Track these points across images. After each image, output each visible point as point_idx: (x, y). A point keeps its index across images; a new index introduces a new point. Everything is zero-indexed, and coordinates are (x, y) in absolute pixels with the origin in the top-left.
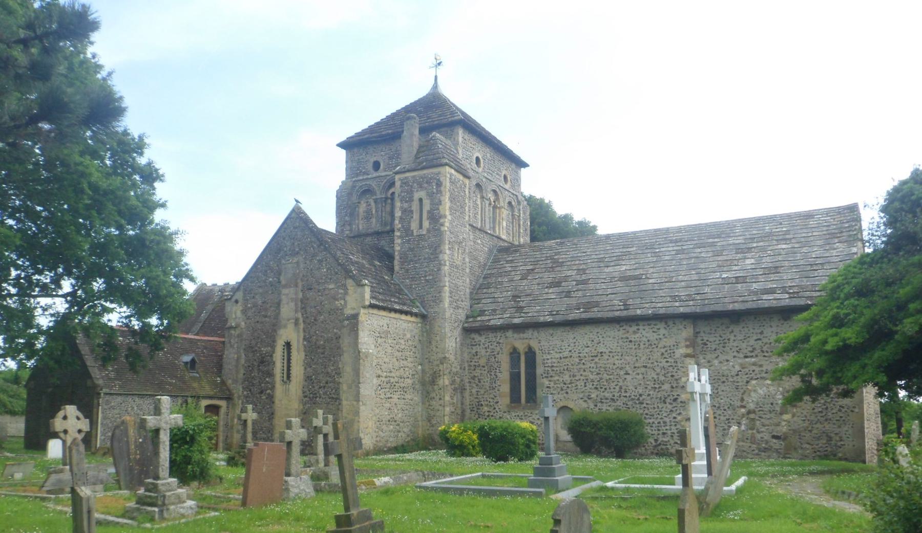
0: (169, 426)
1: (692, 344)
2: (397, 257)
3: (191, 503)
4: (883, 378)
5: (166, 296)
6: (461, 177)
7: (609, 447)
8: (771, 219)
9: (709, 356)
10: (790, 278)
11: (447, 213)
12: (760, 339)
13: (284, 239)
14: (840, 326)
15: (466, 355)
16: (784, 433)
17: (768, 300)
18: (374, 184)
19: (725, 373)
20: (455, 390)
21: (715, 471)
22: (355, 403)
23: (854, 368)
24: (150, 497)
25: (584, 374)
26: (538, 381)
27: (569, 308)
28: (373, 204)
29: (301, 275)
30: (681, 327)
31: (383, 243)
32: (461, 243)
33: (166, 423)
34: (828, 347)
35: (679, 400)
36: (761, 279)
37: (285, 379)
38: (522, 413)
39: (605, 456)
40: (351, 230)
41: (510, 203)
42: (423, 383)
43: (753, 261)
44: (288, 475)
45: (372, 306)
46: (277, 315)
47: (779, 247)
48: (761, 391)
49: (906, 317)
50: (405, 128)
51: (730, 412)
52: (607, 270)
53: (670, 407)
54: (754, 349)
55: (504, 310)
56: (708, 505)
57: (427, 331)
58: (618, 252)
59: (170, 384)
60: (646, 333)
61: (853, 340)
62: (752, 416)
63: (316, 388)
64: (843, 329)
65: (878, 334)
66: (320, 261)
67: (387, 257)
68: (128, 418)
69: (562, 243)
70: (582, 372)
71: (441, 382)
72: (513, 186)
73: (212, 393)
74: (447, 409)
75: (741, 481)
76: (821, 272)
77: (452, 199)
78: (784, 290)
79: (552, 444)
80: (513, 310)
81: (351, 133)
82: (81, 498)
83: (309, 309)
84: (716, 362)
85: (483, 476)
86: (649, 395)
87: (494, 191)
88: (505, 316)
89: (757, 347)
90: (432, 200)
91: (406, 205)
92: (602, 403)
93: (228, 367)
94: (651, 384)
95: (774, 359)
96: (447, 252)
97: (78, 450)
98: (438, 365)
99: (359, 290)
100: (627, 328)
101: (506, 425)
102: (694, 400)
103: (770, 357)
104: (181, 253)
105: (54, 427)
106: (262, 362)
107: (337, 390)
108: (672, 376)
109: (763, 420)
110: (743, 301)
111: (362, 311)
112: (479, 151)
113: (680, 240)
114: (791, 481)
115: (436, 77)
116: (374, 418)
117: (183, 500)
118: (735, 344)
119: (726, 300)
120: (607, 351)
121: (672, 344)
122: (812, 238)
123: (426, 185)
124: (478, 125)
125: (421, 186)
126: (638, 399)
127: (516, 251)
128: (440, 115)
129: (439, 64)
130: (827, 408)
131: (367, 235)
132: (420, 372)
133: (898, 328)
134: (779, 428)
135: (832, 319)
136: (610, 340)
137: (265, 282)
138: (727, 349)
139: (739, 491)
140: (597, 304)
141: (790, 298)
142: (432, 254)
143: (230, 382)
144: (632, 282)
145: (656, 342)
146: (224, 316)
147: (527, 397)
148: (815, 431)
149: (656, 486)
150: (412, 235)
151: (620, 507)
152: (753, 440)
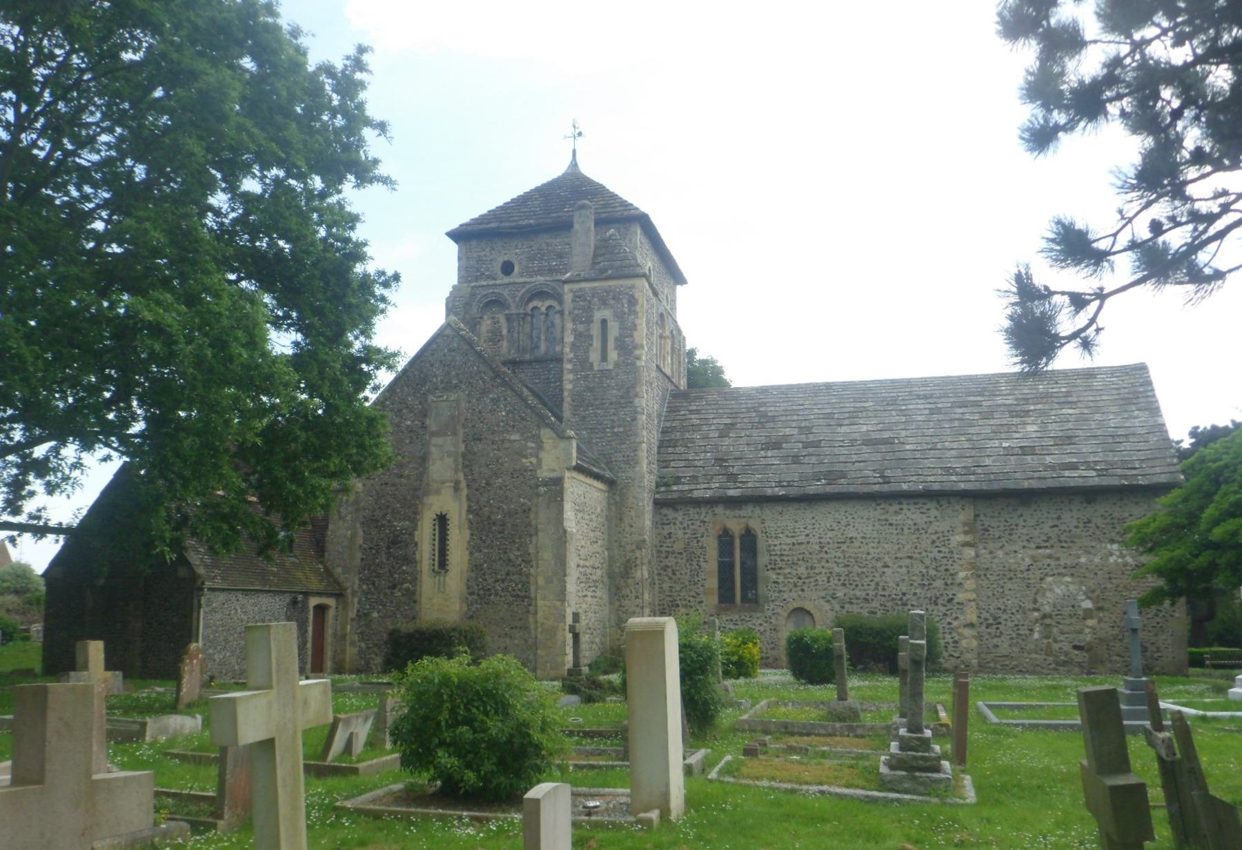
1: (970, 529)
9: (991, 545)
16: (1089, 643)
17: (1073, 478)
18: (506, 293)
19: (1013, 567)
22: (558, 603)
27: (803, 478)
29: (462, 419)
30: (958, 507)
35: (955, 601)
36: (1054, 450)
38: (735, 617)
42: (611, 575)
45: (578, 469)
46: (422, 474)
47: (1064, 411)
48: (1058, 591)
53: (943, 609)
57: (616, 503)
58: (849, 406)
60: (911, 515)
62: (1048, 621)
63: (490, 581)
66: (495, 401)
78: (1088, 466)
80: (724, 479)
83: (476, 469)
84: (1000, 553)
86: (915, 594)
91: (581, 328)
92: (851, 603)
94: (918, 580)
99: (563, 444)
100: (887, 507)
107: (526, 585)
108: (947, 570)
110: (1039, 478)
111: (567, 474)
115: (574, 151)
119: (1018, 475)
121: (945, 529)
123: (612, 302)
125: (604, 303)
129: (580, 134)
134: (1081, 637)
136: (862, 523)
138: (1014, 537)
140: (843, 475)
142: (622, 397)
144: (883, 448)
152: (1049, 651)
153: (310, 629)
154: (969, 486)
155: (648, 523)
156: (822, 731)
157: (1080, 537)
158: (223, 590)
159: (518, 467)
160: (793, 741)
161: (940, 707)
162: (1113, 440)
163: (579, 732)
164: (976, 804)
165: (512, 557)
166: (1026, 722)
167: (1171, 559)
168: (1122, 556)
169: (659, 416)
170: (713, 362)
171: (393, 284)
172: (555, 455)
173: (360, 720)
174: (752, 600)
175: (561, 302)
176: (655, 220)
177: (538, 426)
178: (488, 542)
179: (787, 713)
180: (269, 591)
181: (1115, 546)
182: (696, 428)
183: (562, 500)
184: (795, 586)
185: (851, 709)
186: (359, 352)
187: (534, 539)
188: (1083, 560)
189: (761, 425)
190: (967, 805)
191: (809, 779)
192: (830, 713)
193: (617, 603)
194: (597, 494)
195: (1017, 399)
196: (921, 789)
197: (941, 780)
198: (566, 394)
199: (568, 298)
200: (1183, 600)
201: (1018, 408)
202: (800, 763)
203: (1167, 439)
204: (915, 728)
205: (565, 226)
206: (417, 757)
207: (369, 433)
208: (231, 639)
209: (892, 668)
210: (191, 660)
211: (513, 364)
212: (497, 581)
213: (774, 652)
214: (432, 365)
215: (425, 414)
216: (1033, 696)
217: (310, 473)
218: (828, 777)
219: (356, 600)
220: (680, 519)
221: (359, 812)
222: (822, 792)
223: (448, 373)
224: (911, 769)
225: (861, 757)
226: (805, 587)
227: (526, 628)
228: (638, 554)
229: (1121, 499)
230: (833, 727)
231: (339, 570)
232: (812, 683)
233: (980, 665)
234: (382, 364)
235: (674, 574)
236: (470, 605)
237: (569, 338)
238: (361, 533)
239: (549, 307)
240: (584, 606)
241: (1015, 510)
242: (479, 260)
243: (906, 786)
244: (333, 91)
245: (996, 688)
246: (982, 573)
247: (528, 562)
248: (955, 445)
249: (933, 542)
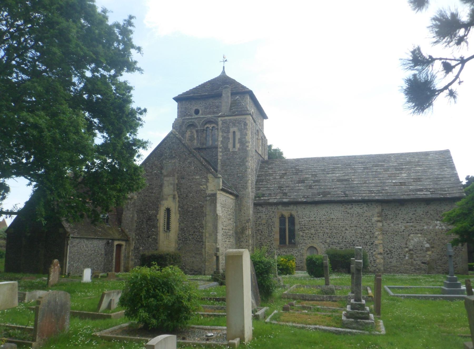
1: (380, 215)
9: (388, 222)
13: (165, 149)
16: (428, 261)
17: (421, 195)
18: (196, 121)
22: (214, 244)
27: (313, 194)
29: (177, 170)
35: (374, 244)
36: (413, 183)
38: (287, 250)
42: (236, 233)
43: (405, 175)
45: (223, 190)
47: (417, 168)
48: (416, 240)
52: (328, 175)
53: (369, 247)
58: (331, 166)
60: (357, 209)
62: (412, 252)
63: (187, 235)
66: (190, 163)
71: (247, 233)
73: (119, 237)
78: (427, 190)
80: (282, 195)
83: (182, 190)
84: (392, 225)
86: (358, 241)
88: (277, 197)
91: (225, 135)
92: (333, 245)
94: (359, 235)
98: (245, 223)
99: (216, 180)
100: (346, 206)
103: (420, 223)
106: (149, 219)
107: (201, 237)
110: (408, 195)
111: (218, 192)
115: (224, 67)
119: (399, 194)
123: (237, 124)
125: (234, 125)
126: (352, 243)
129: (226, 61)
134: (425, 258)
136: (337, 213)
137: (151, 173)
140: (329, 193)
141: (431, 194)
144: (345, 183)
145: (362, 214)
148: (443, 260)
152: (412, 264)
153: (114, 254)
154: (380, 198)
155: (251, 212)
156: (318, 299)
157: (424, 218)
158: (78, 238)
159: (198, 189)
160: (305, 304)
161: (368, 288)
162: (437, 180)
163: (213, 298)
164: (386, 335)
165: (196, 225)
166: (406, 295)
167: (462, 227)
168: (441, 226)
169: (256, 170)
170: (279, 150)
171: (144, 113)
172: (213, 185)
173: (115, 294)
174: (293, 244)
175: (218, 125)
176: (255, 93)
177: (207, 173)
178: (187, 219)
179: (303, 291)
180: (97, 239)
181: (438, 222)
182: (271, 175)
183: (216, 202)
184: (310, 237)
185: (331, 289)
186: (131, 141)
187: (205, 218)
188: (425, 227)
189: (296, 174)
190: (381, 335)
191: (310, 322)
192: (322, 291)
193: (239, 244)
194: (230, 201)
195: (398, 164)
196: (360, 327)
197: (369, 323)
198: (219, 161)
199: (220, 123)
200: (466, 244)
201: (399, 167)
202: (307, 314)
203: (458, 179)
204: (358, 299)
205: (219, 96)
206: (132, 313)
207: (135, 174)
208: (81, 258)
209: (349, 272)
210: (54, 267)
211: (199, 149)
212: (190, 235)
213: (302, 264)
214: (165, 149)
215: (162, 168)
216: (407, 283)
217: (109, 189)
218: (319, 321)
219: (134, 242)
221: (102, 337)
222: (316, 329)
223: (171, 152)
224: (356, 318)
225: (334, 311)
226: (314, 238)
227: (201, 254)
228: (247, 224)
229: (441, 203)
230: (323, 297)
231: (127, 230)
232: (316, 277)
233: (384, 270)
234: (141, 146)
235: (262, 233)
237: (220, 139)
238: (136, 216)
239: (213, 127)
240: (225, 245)
241: (398, 208)
243: (354, 326)
244: (119, 34)
245: (391, 279)
246: (385, 233)
247: (202, 227)
248: (374, 182)
249: (365, 220)
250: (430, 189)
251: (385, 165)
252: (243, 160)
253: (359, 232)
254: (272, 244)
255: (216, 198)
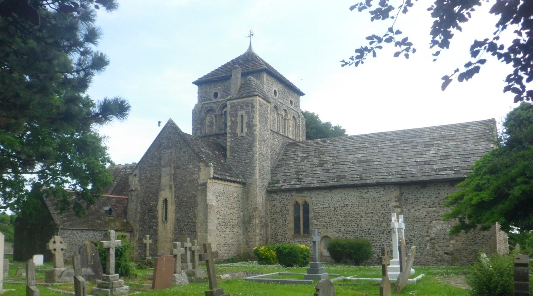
0: (114, 246)
1: (399, 200)
2: (228, 149)
3: (126, 287)
4: (503, 220)
5: (98, 174)
6: (265, 102)
7: (351, 259)
8: (446, 127)
9: (409, 207)
10: (455, 162)
11: (258, 124)
12: (437, 197)
14: (481, 190)
15: (268, 206)
16: (452, 251)
17: (442, 175)
18: (214, 106)
19: (418, 217)
20: (262, 226)
21: (403, 270)
22: (205, 234)
23: (487, 214)
24: (105, 283)
25: (337, 217)
26: (310, 221)
27: (328, 179)
28: (214, 117)
30: (393, 190)
31: (220, 140)
32: (265, 141)
33: (113, 245)
34: (473, 202)
36: (439, 162)
37: (164, 220)
39: (349, 264)
40: (201, 133)
41: (294, 117)
42: (244, 223)
43: (434, 152)
44: (175, 273)
45: (214, 178)
46: (160, 183)
48: (438, 227)
49: (516, 186)
50: (233, 74)
51: (420, 239)
52: (350, 157)
53: (386, 236)
54: (434, 203)
55: (290, 180)
56: (399, 287)
57: (246, 192)
58: (357, 146)
59: (97, 223)
60: (372, 194)
61: (486, 199)
62: (433, 241)
64: (482, 192)
65: (500, 195)
66: (184, 152)
67: (223, 149)
68: (87, 242)
69: (324, 141)
70: (336, 216)
71: (254, 222)
72: (295, 107)
73: (121, 228)
74: (258, 238)
75: (420, 277)
76: (472, 159)
77: (260, 116)
78: (451, 169)
79: (317, 257)
80: (296, 180)
81: (201, 76)
82: (79, 282)
84: (413, 210)
85: (280, 274)
86: (374, 229)
87: (285, 110)
88: (291, 183)
89: (436, 202)
90: (249, 116)
91: (233, 119)
92: (347, 234)
93: (130, 213)
94: (375, 223)
95: (446, 209)
96: (258, 146)
97: (77, 258)
98: (252, 212)
99: (207, 169)
100: (362, 190)
101: (292, 246)
102: (394, 232)
104: (105, 148)
105: (48, 247)
106: (150, 210)
107: (194, 226)
109: (439, 244)
111: (209, 181)
112: (276, 86)
113: (393, 140)
114: (451, 277)
115: (250, 43)
116: (216, 243)
117: (123, 286)
118: (424, 200)
119: (419, 175)
120: (350, 204)
122: (468, 139)
123: (245, 107)
124: (275, 71)
125: (242, 108)
126: (368, 232)
127: (297, 145)
128: (253, 66)
129: (252, 35)
130: (475, 237)
131: (211, 136)
132: (242, 216)
133: (511, 192)
134: (448, 248)
135: (476, 186)
136: (352, 198)
138: (419, 203)
139: (418, 281)
140: (344, 177)
141: (455, 173)
143: (132, 222)
144: (365, 164)
146: (128, 183)
147: (304, 230)
148: (469, 250)
149: (373, 279)
150: (237, 136)
151: (353, 289)
159: (192, 179)
215: (160, 159)
219: (138, 233)
220: (278, 198)
223: (168, 142)
226: (328, 227)
236: (176, 235)
238: (139, 207)
242: (206, 93)
247: (195, 217)
250: (455, 167)
251: (447, 141)
252: (251, 145)
253: (375, 219)
254: (287, 234)
255: (206, 187)
